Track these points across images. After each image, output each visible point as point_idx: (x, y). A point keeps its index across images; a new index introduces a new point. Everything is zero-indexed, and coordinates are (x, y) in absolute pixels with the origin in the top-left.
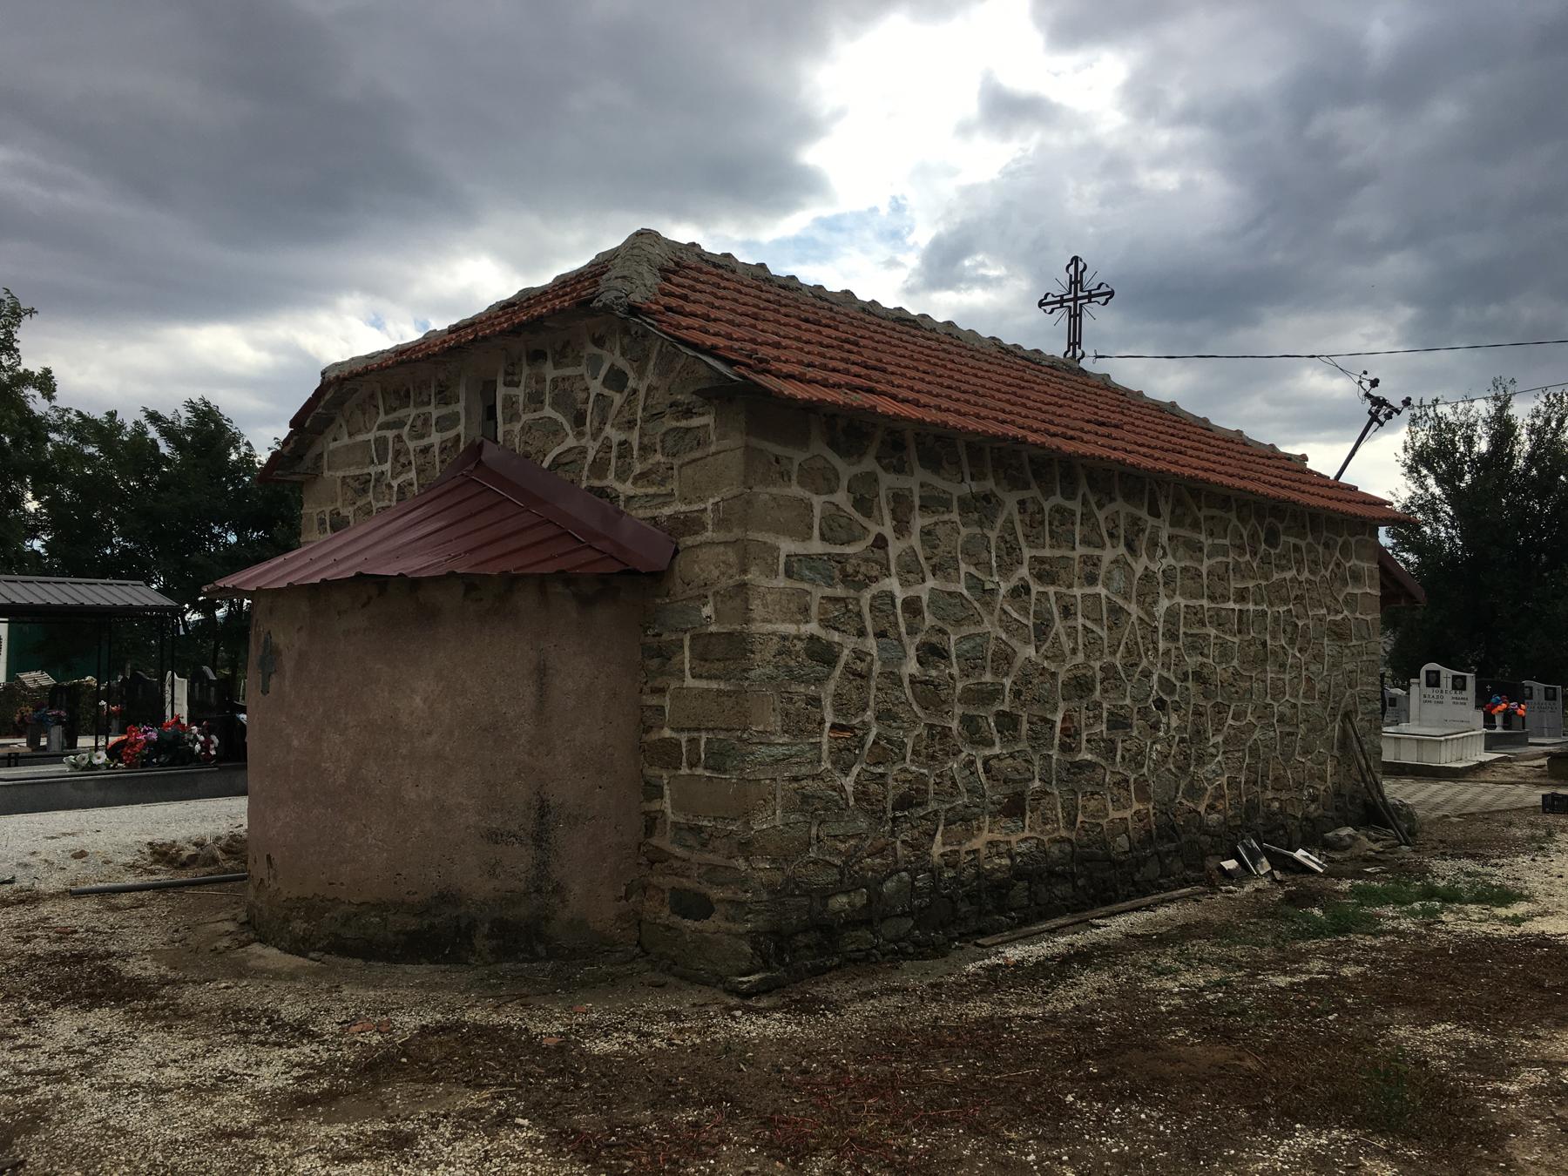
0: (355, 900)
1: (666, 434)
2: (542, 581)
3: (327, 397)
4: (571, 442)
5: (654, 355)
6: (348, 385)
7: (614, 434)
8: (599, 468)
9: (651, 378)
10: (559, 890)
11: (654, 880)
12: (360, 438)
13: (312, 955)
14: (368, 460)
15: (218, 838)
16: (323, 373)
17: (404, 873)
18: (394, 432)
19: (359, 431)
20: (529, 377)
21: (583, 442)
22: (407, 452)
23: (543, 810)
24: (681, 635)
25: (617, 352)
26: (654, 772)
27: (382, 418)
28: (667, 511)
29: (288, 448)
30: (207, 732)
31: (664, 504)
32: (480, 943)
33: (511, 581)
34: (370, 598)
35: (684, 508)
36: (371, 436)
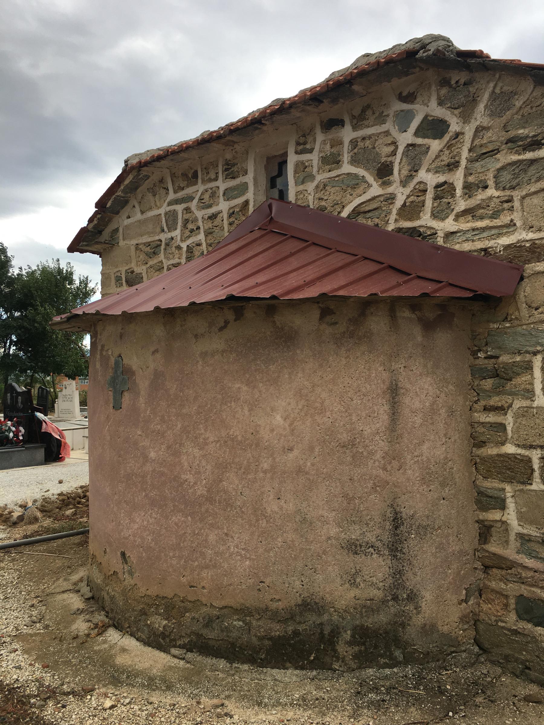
0: (217, 603)
1: (503, 168)
2: (393, 305)
3: (127, 182)
4: (376, 190)
5: (486, 96)
6: (145, 171)
7: (430, 179)
8: (411, 210)
9: (480, 116)
10: (412, 597)
11: (493, 584)
12: (151, 214)
13: (174, 651)
14: (158, 230)
15: (35, 501)
16: (126, 162)
17: (268, 580)
18: (184, 206)
19: (151, 209)
20: (324, 142)
21: (390, 190)
22: (196, 220)
23: (397, 521)
24: (528, 357)
25: (433, 103)
26: (491, 485)
27: (172, 196)
28: (505, 241)
29: (92, 225)
30: (17, 425)
31: (499, 235)
32: (342, 648)
33: (367, 304)
34: (227, 323)
35: (531, 236)
36: (162, 211)
